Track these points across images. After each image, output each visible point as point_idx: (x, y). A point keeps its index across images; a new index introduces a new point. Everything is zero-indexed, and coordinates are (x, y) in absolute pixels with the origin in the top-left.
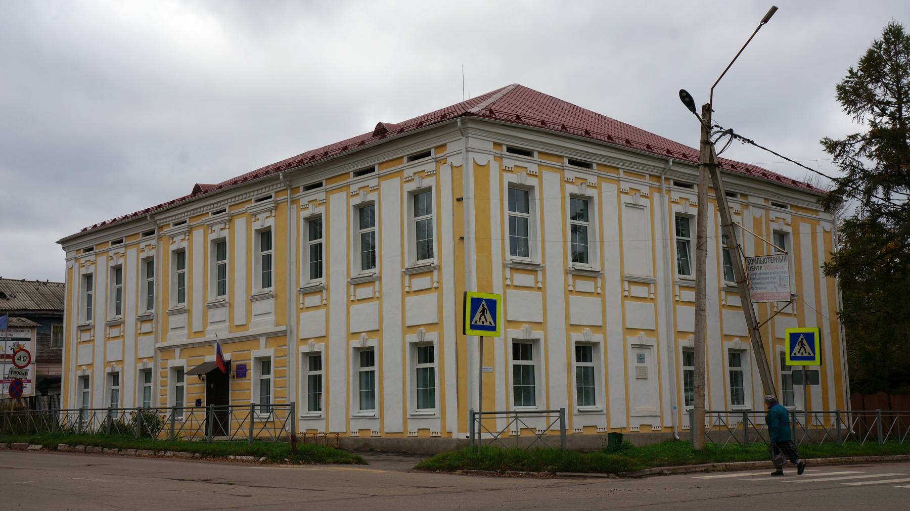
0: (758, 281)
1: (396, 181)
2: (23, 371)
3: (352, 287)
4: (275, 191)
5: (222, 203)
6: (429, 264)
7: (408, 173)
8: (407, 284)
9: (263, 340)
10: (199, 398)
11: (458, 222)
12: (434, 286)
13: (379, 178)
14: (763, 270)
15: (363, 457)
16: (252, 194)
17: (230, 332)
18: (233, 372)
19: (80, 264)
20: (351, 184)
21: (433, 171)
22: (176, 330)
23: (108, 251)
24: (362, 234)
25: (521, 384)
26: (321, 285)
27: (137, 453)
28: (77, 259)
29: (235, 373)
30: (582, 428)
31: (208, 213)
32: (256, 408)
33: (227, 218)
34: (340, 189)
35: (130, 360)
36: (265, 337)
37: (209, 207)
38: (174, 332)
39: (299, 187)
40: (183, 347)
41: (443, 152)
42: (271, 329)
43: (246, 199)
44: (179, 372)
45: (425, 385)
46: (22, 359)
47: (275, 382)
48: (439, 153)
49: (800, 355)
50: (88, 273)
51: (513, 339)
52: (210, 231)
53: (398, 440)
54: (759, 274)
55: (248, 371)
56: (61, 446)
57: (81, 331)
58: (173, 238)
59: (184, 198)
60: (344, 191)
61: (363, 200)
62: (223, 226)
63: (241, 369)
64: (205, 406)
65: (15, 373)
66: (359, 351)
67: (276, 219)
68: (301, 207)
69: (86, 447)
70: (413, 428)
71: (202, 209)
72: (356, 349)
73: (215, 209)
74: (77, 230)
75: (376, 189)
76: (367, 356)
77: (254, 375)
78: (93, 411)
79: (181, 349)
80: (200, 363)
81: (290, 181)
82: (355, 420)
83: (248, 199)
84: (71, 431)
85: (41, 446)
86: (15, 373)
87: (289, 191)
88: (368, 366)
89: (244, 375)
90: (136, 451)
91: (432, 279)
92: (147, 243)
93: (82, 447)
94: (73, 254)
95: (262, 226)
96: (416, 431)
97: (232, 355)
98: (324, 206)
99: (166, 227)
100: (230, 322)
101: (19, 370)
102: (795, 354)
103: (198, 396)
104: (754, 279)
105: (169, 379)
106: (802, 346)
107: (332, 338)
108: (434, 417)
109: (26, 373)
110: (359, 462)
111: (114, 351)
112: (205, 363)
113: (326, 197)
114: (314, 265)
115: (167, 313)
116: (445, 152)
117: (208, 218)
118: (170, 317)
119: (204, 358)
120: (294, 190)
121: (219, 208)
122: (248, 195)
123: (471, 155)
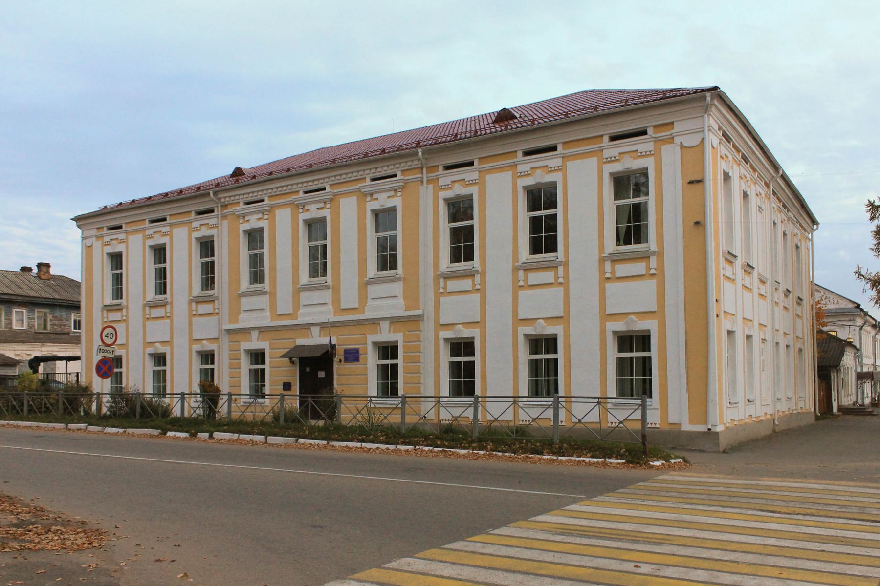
4: (269, 195)
5: (321, 181)
7: (195, 224)
8: (105, 316)
13: (563, 157)
18: (339, 355)
21: (650, 152)
22: (253, 312)
24: (616, 206)
31: (298, 192)
32: (186, 396)
33: (330, 197)
34: (501, 169)
39: (438, 166)
40: (262, 330)
41: (670, 131)
43: (357, 178)
44: (258, 356)
45: (257, 381)
51: (613, 331)
59: (167, 194)
63: (644, 343)
64: (298, 393)
66: (527, 337)
68: (440, 187)
73: (309, 187)
74: (94, 207)
76: (160, 359)
77: (372, 361)
78: (369, 399)
80: (292, 346)
83: (236, 201)
84: (251, 423)
85: (623, 461)
86: (104, 351)
88: (644, 351)
89: (357, 359)
97: (337, 341)
101: (107, 348)
103: (286, 380)
111: (158, 332)
114: (158, 285)
119: (295, 342)
120: (432, 169)
121: (254, 198)
122: (361, 173)
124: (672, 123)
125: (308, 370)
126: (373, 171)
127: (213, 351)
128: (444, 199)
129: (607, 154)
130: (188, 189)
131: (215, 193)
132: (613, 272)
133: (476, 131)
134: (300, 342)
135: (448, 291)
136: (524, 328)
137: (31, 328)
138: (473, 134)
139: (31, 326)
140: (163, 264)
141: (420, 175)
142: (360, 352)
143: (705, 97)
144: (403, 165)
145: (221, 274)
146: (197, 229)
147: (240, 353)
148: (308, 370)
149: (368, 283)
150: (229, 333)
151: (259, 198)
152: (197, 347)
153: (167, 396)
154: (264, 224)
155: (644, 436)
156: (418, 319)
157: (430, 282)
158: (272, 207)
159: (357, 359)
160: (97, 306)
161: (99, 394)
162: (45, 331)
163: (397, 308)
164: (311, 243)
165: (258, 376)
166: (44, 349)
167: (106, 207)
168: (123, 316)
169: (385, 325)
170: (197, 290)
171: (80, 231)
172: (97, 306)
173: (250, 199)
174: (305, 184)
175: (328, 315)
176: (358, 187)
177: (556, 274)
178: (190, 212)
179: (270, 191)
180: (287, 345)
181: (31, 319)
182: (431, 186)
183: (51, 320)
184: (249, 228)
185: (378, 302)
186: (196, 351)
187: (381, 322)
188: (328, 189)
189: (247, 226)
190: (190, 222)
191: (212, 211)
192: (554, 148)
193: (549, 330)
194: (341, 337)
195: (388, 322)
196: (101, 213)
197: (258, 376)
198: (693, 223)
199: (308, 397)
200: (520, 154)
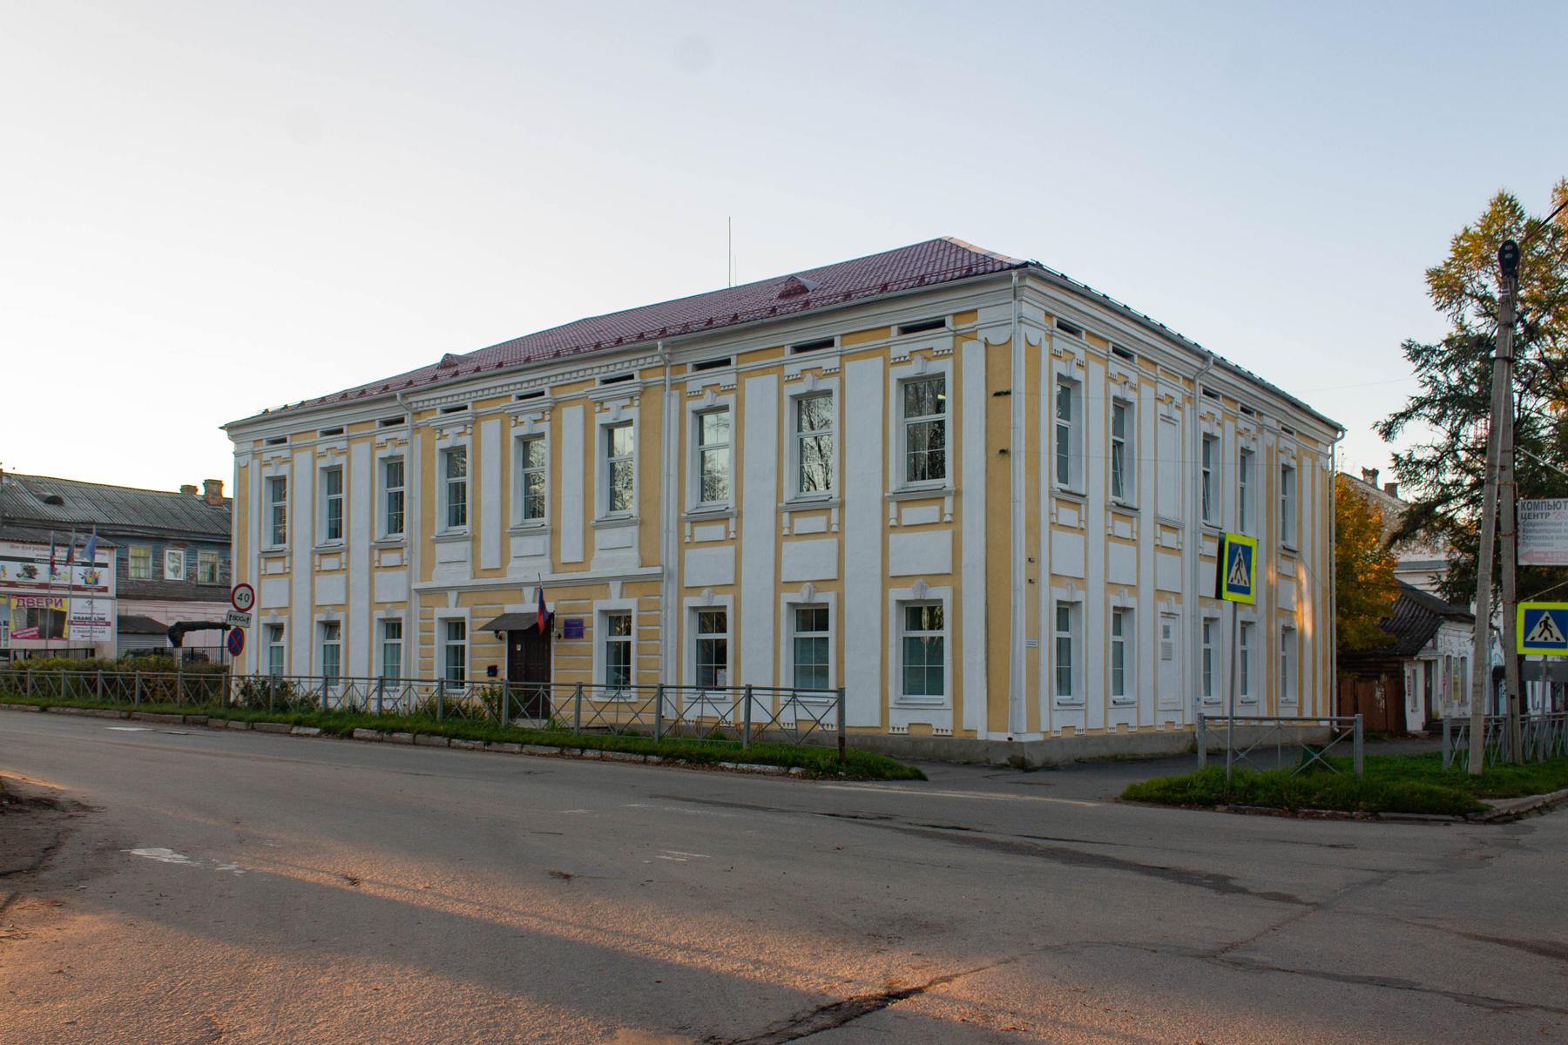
0: (1536, 534)
1: (772, 379)
2: (244, 616)
3: (317, 557)
6: (941, 487)
7: (380, 439)
8: (262, 567)
9: (615, 587)
10: (494, 664)
11: (995, 427)
12: (945, 520)
14: (1551, 519)
15: (925, 770)
16: (596, 371)
17: (553, 573)
18: (558, 629)
19: (261, 462)
20: (787, 364)
21: (949, 350)
23: (316, 445)
25: (815, 667)
26: (727, 511)
27: (524, 750)
28: (255, 454)
29: (563, 630)
30: (1115, 726)
33: (548, 405)
34: (764, 371)
35: (359, 605)
36: (620, 582)
37: (512, 387)
38: (445, 567)
39: (685, 364)
40: (462, 591)
42: (633, 569)
44: (456, 628)
46: (243, 597)
47: (639, 646)
48: (744, 362)
49: (1542, 639)
50: (278, 475)
52: (513, 423)
53: (873, 738)
54: (1541, 524)
55: (587, 629)
56: (358, 733)
57: (266, 558)
58: (441, 430)
60: (772, 373)
61: (810, 388)
62: (461, 429)
65: (235, 618)
67: (641, 411)
69: (415, 736)
70: (900, 721)
71: (456, 398)
72: (381, 620)
73: (523, 390)
75: (838, 372)
76: (813, 618)
77: (598, 635)
78: (350, 681)
79: (459, 593)
81: (670, 354)
82: (900, 711)
83: (505, 394)
86: (235, 618)
87: (668, 369)
88: (457, 638)
89: (580, 635)
90: (522, 747)
91: (942, 510)
92: (276, 454)
93: (406, 736)
94: (248, 447)
95: (615, 419)
96: (906, 726)
97: (556, 606)
98: (734, 395)
99: (426, 414)
100: (551, 557)
101: (240, 615)
102: (1533, 638)
103: (491, 662)
104: (1531, 531)
105: (436, 634)
106: (1547, 626)
107: (746, 589)
108: (943, 707)
109: (248, 619)
110: (919, 777)
111: (330, 591)
112: (505, 614)
113: (737, 381)
115: (433, 540)
116: (975, 323)
117: (508, 404)
118: (437, 545)
119: (503, 608)
122: (589, 372)
123: (1024, 328)
124: (975, 311)
125: (519, 648)
126: (604, 369)
127: (464, 618)
128: (693, 412)
129: (895, 352)
130: (374, 386)
131: (404, 396)
132: (899, 518)
133: (970, 269)
134: (510, 609)
135: (696, 540)
136: (788, 594)
137: (191, 578)
138: (964, 272)
139: (191, 575)
140: (399, 488)
141: (663, 378)
142: (585, 625)
143: (1010, 278)
144: (641, 362)
145: (412, 512)
146: (382, 446)
147: (433, 624)
148: (519, 648)
149: (595, 528)
150: (420, 595)
151: (460, 403)
152: (380, 614)
153: (341, 680)
154: (465, 441)
155: (842, 740)
156: (656, 579)
157: (673, 526)
158: (477, 418)
159: (580, 635)
160: (253, 552)
161: (581, 686)
162: (213, 584)
163: (628, 563)
164: (911, 419)
165: (456, 655)
166: (209, 610)
167: (267, 411)
168: (285, 568)
169: (615, 587)
170: (381, 532)
171: (232, 444)
172: (253, 552)
173: (449, 406)
174: (518, 386)
175: (540, 570)
176: (583, 392)
177: (942, 510)
178: (374, 420)
179: (474, 394)
180: (491, 613)
181: (192, 565)
182: (676, 393)
183: (221, 567)
184: (448, 446)
185: (525, 562)
186: (440, 619)
187: (449, 593)
188: (547, 394)
189: (446, 444)
190: (315, 445)
191: (401, 421)
192: (829, 343)
193: (718, 601)
194: (562, 602)
195: (619, 583)
196: (276, 415)
197: (456, 655)
198: (998, 452)
199: (538, 687)
200: (788, 350)
